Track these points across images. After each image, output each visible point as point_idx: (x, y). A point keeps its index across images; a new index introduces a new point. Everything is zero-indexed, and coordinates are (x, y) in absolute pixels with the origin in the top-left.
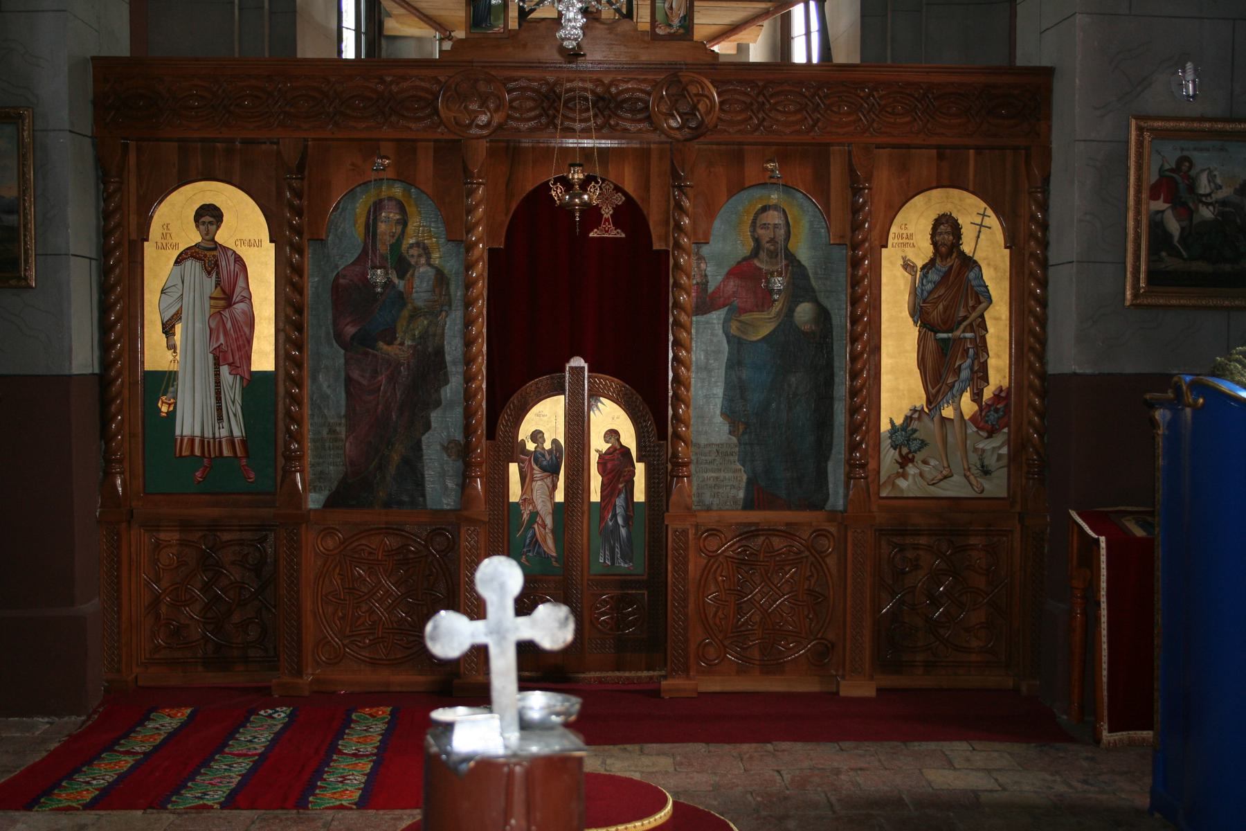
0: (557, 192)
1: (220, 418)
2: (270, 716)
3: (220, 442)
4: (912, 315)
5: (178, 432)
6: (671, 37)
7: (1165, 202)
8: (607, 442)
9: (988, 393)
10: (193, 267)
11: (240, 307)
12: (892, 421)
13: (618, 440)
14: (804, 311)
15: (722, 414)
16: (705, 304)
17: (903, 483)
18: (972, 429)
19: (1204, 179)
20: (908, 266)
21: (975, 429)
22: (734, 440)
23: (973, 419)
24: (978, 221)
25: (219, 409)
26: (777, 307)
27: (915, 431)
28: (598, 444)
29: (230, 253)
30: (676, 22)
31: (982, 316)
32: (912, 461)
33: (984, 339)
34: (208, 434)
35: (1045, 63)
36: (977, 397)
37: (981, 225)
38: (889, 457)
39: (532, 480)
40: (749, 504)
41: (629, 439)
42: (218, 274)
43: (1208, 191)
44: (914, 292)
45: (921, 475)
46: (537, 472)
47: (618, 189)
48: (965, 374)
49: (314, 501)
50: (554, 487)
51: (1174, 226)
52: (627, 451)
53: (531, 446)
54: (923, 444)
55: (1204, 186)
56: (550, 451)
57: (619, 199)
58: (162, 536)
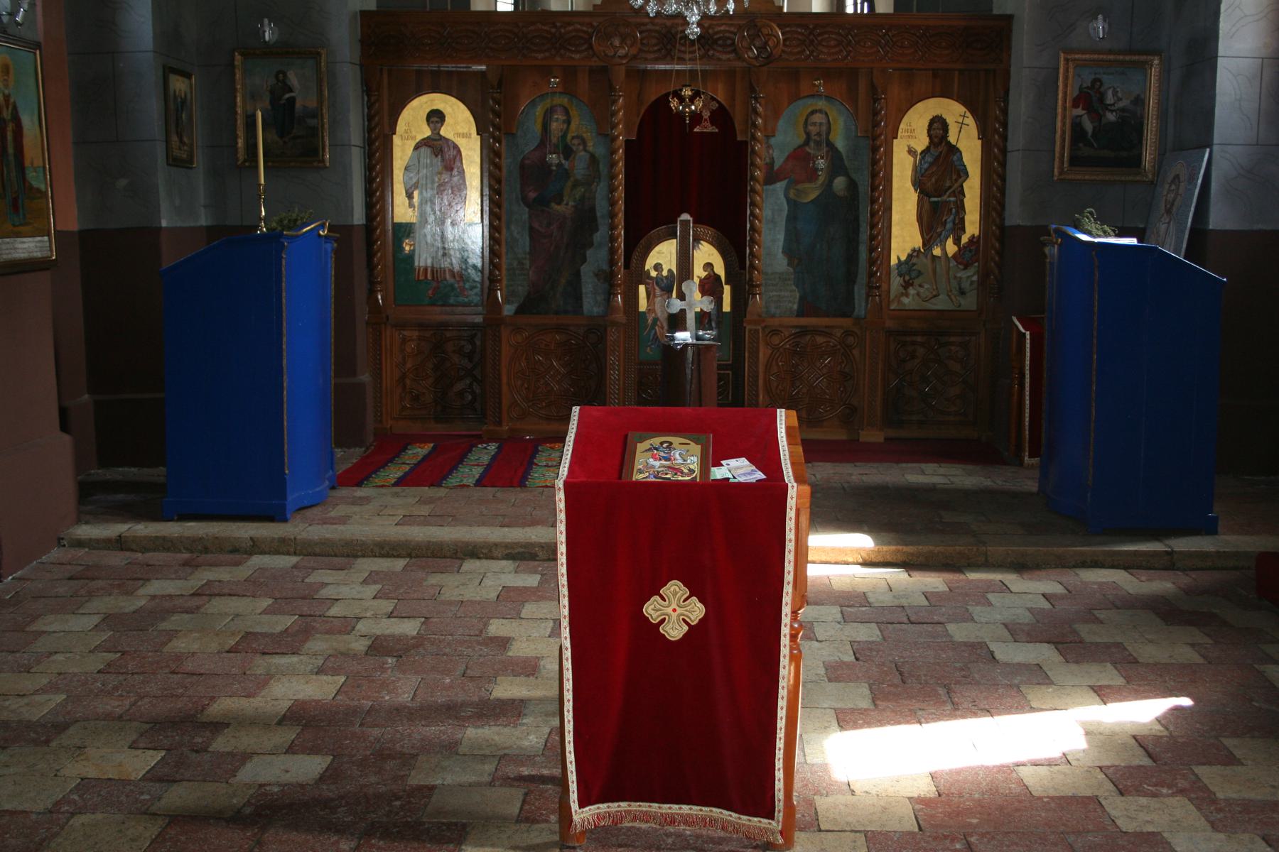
0: (674, 104)
2: (485, 448)
4: (914, 184)
5: (416, 264)
7: (1083, 109)
8: (705, 271)
9: (965, 239)
12: (898, 258)
13: (713, 269)
14: (840, 183)
16: (771, 178)
17: (906, 300)
18: (953, 263)
19: (1110, 93)
20: (911, 152)
23: (954, 256)
26: (821, 180)
27: (914, 264)
28: (699, 272)
31: (962, 186)
32: (912, 285)
35: (1008, 12)
36: (957, 241)
38: (896, 282)
39: (655, 296)
40: (801, 314)
41: (720, 269)
42: (442, 156)
43: (1112, 102)
44: (915, 169)
46: (658, 291)
48: (949, 226)
51: (1088, 126)
52: (718, 277)
53: (654, 274)
54: (920, 273)
55: (1110, 99)
57: (714, 106)
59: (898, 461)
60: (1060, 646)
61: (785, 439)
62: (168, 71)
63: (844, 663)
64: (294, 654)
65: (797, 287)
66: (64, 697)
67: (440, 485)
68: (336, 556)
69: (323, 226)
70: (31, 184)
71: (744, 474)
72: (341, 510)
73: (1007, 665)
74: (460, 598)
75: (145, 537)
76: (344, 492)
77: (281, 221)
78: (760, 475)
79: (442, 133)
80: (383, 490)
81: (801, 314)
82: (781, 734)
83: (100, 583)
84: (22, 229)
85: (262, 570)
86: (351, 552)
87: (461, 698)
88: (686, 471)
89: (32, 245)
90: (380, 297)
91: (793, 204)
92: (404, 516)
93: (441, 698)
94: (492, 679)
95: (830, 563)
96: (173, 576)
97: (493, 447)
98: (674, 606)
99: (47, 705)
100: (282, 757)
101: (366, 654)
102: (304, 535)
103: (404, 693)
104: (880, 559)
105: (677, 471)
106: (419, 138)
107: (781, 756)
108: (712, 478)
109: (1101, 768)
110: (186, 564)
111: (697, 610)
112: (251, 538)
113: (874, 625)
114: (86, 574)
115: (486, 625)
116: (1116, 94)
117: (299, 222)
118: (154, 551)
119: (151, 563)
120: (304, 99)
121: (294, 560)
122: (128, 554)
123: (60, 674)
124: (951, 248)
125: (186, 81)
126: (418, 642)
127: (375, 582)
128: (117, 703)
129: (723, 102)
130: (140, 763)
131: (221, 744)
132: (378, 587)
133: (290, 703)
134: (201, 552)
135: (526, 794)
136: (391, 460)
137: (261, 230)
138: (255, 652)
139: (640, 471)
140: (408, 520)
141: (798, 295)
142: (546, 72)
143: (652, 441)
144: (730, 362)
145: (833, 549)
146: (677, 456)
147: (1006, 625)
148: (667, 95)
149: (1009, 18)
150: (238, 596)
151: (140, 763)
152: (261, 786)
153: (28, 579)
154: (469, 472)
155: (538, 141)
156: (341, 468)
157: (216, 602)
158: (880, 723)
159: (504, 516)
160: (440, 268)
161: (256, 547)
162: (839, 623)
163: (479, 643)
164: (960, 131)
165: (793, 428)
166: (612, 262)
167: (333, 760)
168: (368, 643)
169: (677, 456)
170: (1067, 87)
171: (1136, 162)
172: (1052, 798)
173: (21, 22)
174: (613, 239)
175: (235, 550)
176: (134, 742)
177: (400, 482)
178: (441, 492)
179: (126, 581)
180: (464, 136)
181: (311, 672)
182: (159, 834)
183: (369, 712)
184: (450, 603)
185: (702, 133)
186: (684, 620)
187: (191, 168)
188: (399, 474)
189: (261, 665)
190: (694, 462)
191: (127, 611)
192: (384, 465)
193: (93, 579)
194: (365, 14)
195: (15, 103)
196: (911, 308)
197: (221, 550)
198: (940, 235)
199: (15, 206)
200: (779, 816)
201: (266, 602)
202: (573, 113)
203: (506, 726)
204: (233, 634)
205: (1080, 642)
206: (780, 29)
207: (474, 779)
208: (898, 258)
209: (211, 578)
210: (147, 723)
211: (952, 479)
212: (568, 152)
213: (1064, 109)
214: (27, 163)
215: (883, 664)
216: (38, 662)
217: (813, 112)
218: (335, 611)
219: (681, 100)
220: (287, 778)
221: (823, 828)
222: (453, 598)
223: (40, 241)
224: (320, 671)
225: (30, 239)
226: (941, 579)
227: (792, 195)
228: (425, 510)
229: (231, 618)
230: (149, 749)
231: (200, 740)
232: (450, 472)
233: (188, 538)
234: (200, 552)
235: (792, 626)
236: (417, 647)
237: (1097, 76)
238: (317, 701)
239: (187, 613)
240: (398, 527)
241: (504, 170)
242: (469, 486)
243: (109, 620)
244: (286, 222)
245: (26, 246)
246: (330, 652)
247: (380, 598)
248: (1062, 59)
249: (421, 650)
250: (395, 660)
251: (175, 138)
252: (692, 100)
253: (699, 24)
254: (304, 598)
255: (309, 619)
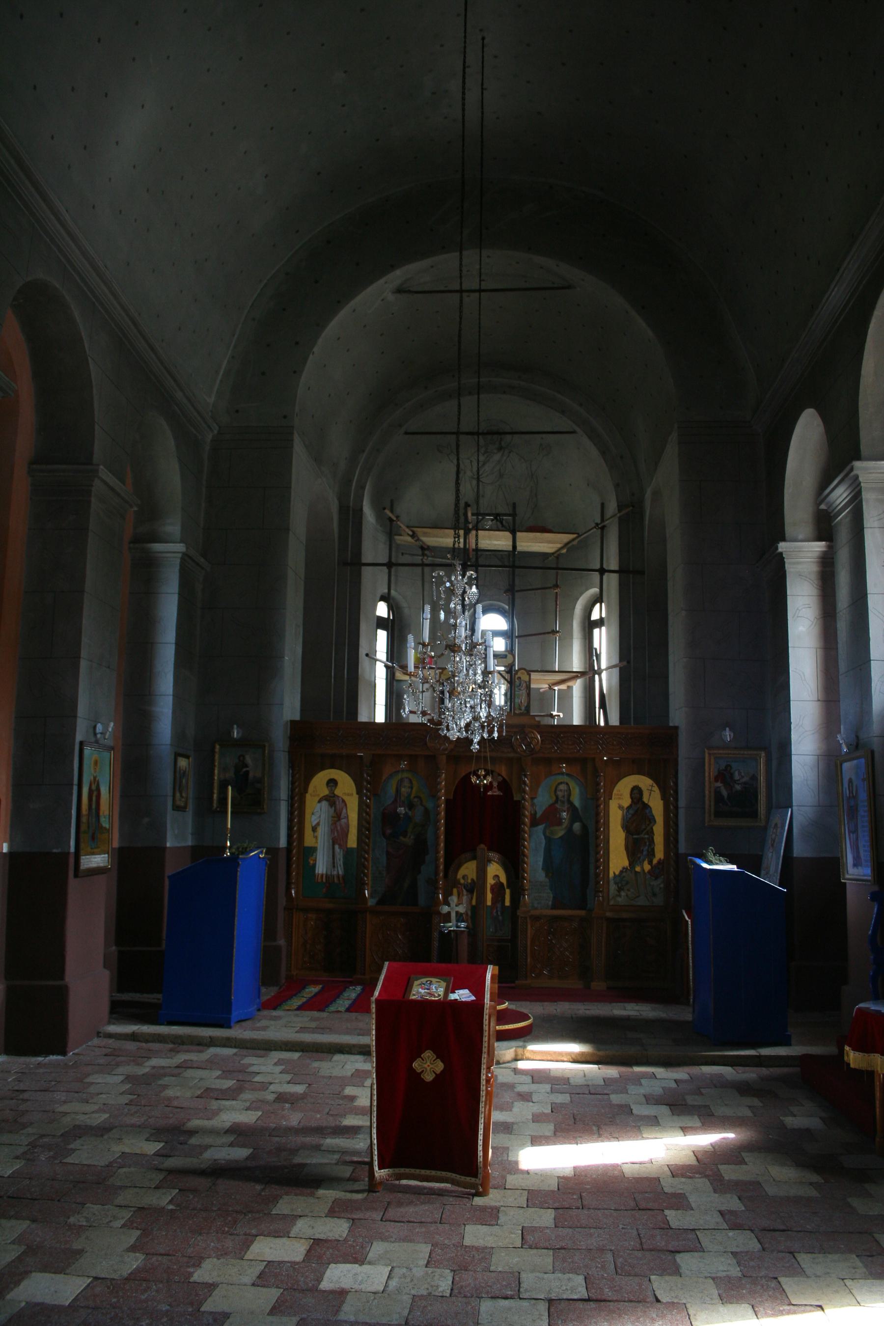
0: (474, 779)
1: (334, 867)
2: (354, 989)
3: (334, 877)
4: (623, 828)
5: (317, 872)
6: (521, 714)
7: (721, 783)
8: (494, 880)
9: (655, 861)
10: (325, 804)
11: (343, 821)
12: (614, 873)
13: (499, 879)
14: (577, 826)
15: (542, 869)
16: (535, 823)
17: (619, 899)
18: (648, 876)
19: (736, 773)
20: (620, 807)
21: (649, 876)
22: (547, 880)
23: (649, 872)
24: (650, 788)
25: (334, 863)
26: (564, 826)
27: (624, 877)
28: (490, 881)
29: (340, 799)
30: (523, 708)
31: (652, 829)
32: (623, 890)
33: (653, 838)
34: (329, 873)
35: (676, 725)
36: (650, 863)
37: (651, 790)
38: (613, 888)
39: (463, 895)
40: (554, 907)
41: (503, 879)
42: (335, 807)
43: (738, 778)
44: (623, 819)
45: (627, 895)
46: (465, 892)
47: (499, 775)
48: (645, 853)
49: (371, 902)
50: (472, 898)
51: (725, 793)
52: (502, 884)
53: (462, 881)
54: (627, 883)
55: (737, 776)
56: (470, 884)
57: (500, 779)
58: (310, 915)
59: (611, 1002)
60: (672, 1107)
61: (489, 980)
62: (177, 755)
63: (544, 1113)
64: (233, 1100)
65: (551, 890)
66: (108, 1115)
67: (323, 1011)
68: (259, 1049)
69: (262, 852)
70: (101, 825)
71: (466, 998)
72: (264, 1023)
73: (638, 1116)
74: (330, 1075)
75: (148, 1034)
76: (265, 1012)
77: (238, 848)
78: (473, 998)
79: (336, 792)
80: (290, 1013)
81: (554, 907)
82: (481, 1132)
83: (122, 1059)
84: (96, 850)
85: (216, 1055)
86: (266, 1047)
87: (325, 1124)
88: (437, 995)
89: (99, 859)
90: (293, 892)
91: (549, 840)
92: (301, 1028)
93: (313, 1124)
94: (344, 1116)
95: (553, 1061)
96: (164, 1056)
97: (359, 989)
98: (428, 1063)
99: (102, 1118)
100: (227, 1148)
101: (274, 1101)
102: (241, 1036)
103: (294, 1121)
104: (583, 1059)
105: (431, 995)
106: (322, 795)
107: (481, 1144)
108: (449, 999)
109: (668, 1165)
110: (171, 1050)
111: (440, 1066)
112: (210, 1037)
113: (568, 1095)
114: (113, 1053)
115: (343, 1089)
116: (740, 774)
117: (248, 850)
118: (152, 1042)
119: (151, 1049)
120: (254, 772)
121: (234, 1050)
122: (138, 1043)
123: (104, 1104)
124: (647, 867)
125: (187, 760)
126: (304, 1096)
127: (281, 1065)
128: (137, 1120)
129: (505, 776)
130: (152, 1148)
131: (194, 1141)
132: (283, 1067)
133: (231, 1124)
134: (180, 1044)
135: (354, 1169)
136: (295, 995)
137: (227, 854)
138: (212, 1098)
139: (414, 995)
140: (303, 1030)
141: (551, 895)
142: (399, 758)
143: (422, 980)
144: (510, 938)
145: (555, 1053)
146: (434, 988)
147: (645, 1096)
148: (470, 773)
149: (676, 728)
150: (202, 1069)
151: (152, 1148)
152: (215, 1160)
153: (82, 1055)
154: (343, 1003)
155: (392, 799)
156: (264, 998)
157: (189, 1071)
158: (555, 1143)
159: (361, 1029)
160: (331, 875)
161: (212, 1042)
162: (548, 1093)
163: (338, 1098)
164: (650, 795)
165: (495, 975)
166: (437, 873)
167: (253, 1151)
168: (275, 1096)
169: (434, 988)
170: (710, 771)
171: (754, 815)
172: (634, 1178)
173: (112, 744)
174: (437, 859)
175: (199, 1044)
176: (147, 1138)
177: (300, 1008)
178: (324, 1015)
179: (138, 1059)
180: (348, 795)
181: (243, 1109)
182: (164, 1178)
183: (274, 1129)
184: (324, 1077)
185: (492, 795)
186: (433, 1071)
187: (185, 811)
188: (299, 1003)
189: (215, 1105)
190: (441, 991)
191: (139, 1074)
192: (291, 997)
193: (119, 1056)
194: (293, 722)
195: (98, 781)
196: (623, 904)
197: (192, 1044)
198: (639, 858)
199: (93, 838)
200: (480, 1176)
201: (219, 1073)
202: (414, 782)
203: (348, 1138)
204: (199, 1088)
205: (685, 1105)
206: (539, 734)
207: (327, 1161)
208: (614, 873)
209: (186, 1058)
210: (154, 1129)
211: (642, 1013)
212: (411, 806)
213: (710, 782)
214: (101, 813)
215: (566, 1115)
216: (92, 1098)
217: (561, 783)
218: (257, 1079)
219: (478, 777)
220: (228, 1157)
221: (507, 1187)
222: (326, 1075)
223: (104, 857)
224: (247, 1109)
225: (99, 856)
226: (617, 1071)
227: (548, 834)
228: (313, 1025)
229: (197, 1080)
230: (156, 1141)
231: (182, 1139)
232: (331, 1003)
233: (173, 1035)
234: (179, 1042)
235: (487, 1076)
236: (303, 1099)
237: (728, 763)
238: (246, 1123)
239: (173, 1076)
240: (296, 1034)
241: (372, 816)
242: (341, 1012)
243: (128, 1078)
244: (240, 849)
245: (96, 860)
246: (254, 1099)
247: (284, 1073)
248: (707, 755)
249: (305, 1101)
250: (290, 1105)
251: (178, 795)
252: (485, 777)
253: (479, 743)
254: (240, 1071)
255: (242, 1083)
